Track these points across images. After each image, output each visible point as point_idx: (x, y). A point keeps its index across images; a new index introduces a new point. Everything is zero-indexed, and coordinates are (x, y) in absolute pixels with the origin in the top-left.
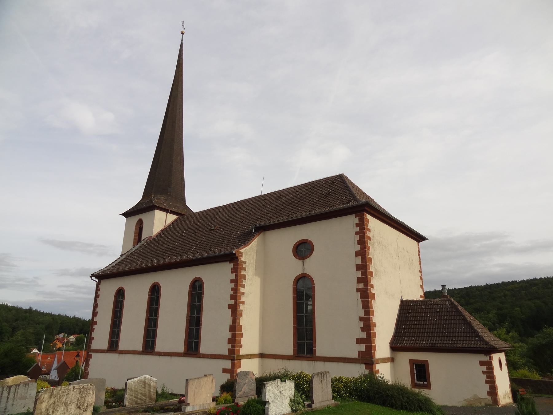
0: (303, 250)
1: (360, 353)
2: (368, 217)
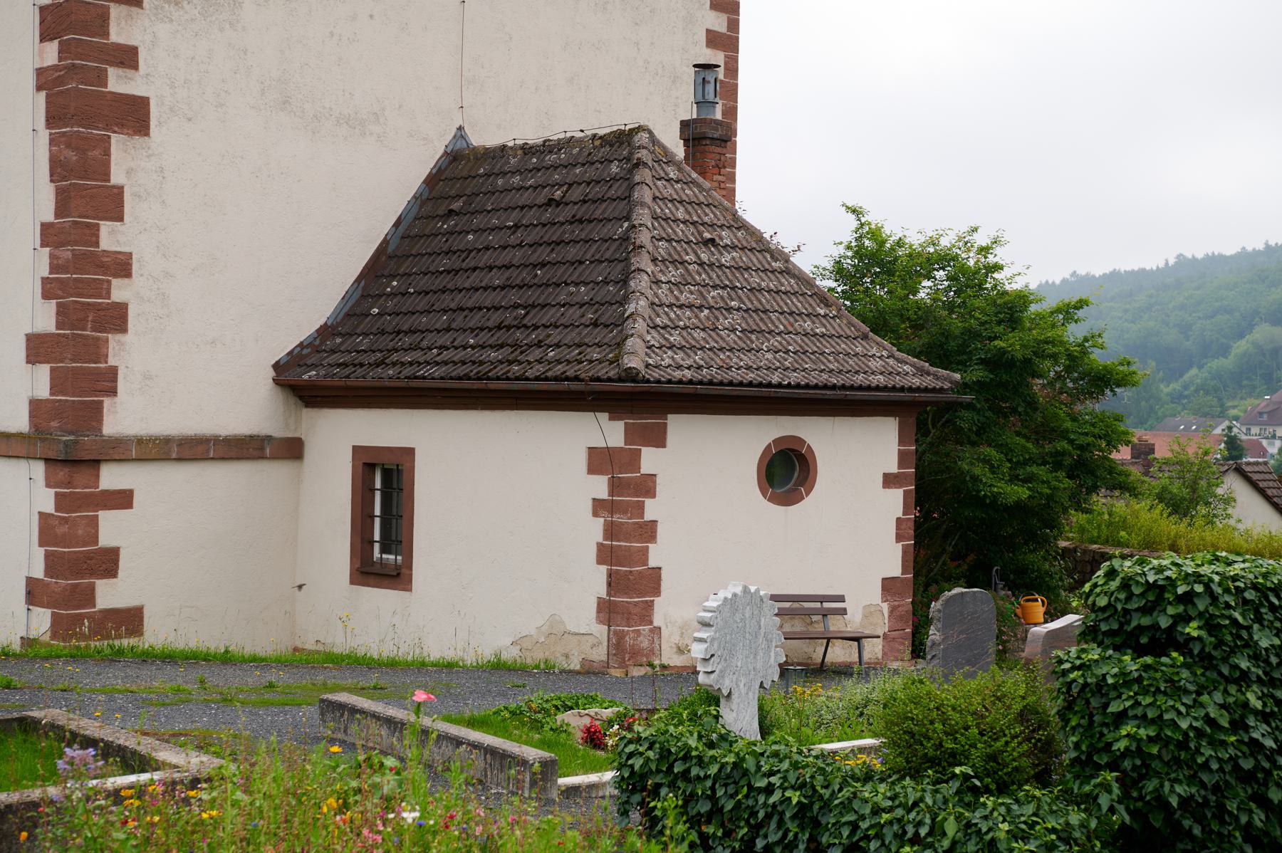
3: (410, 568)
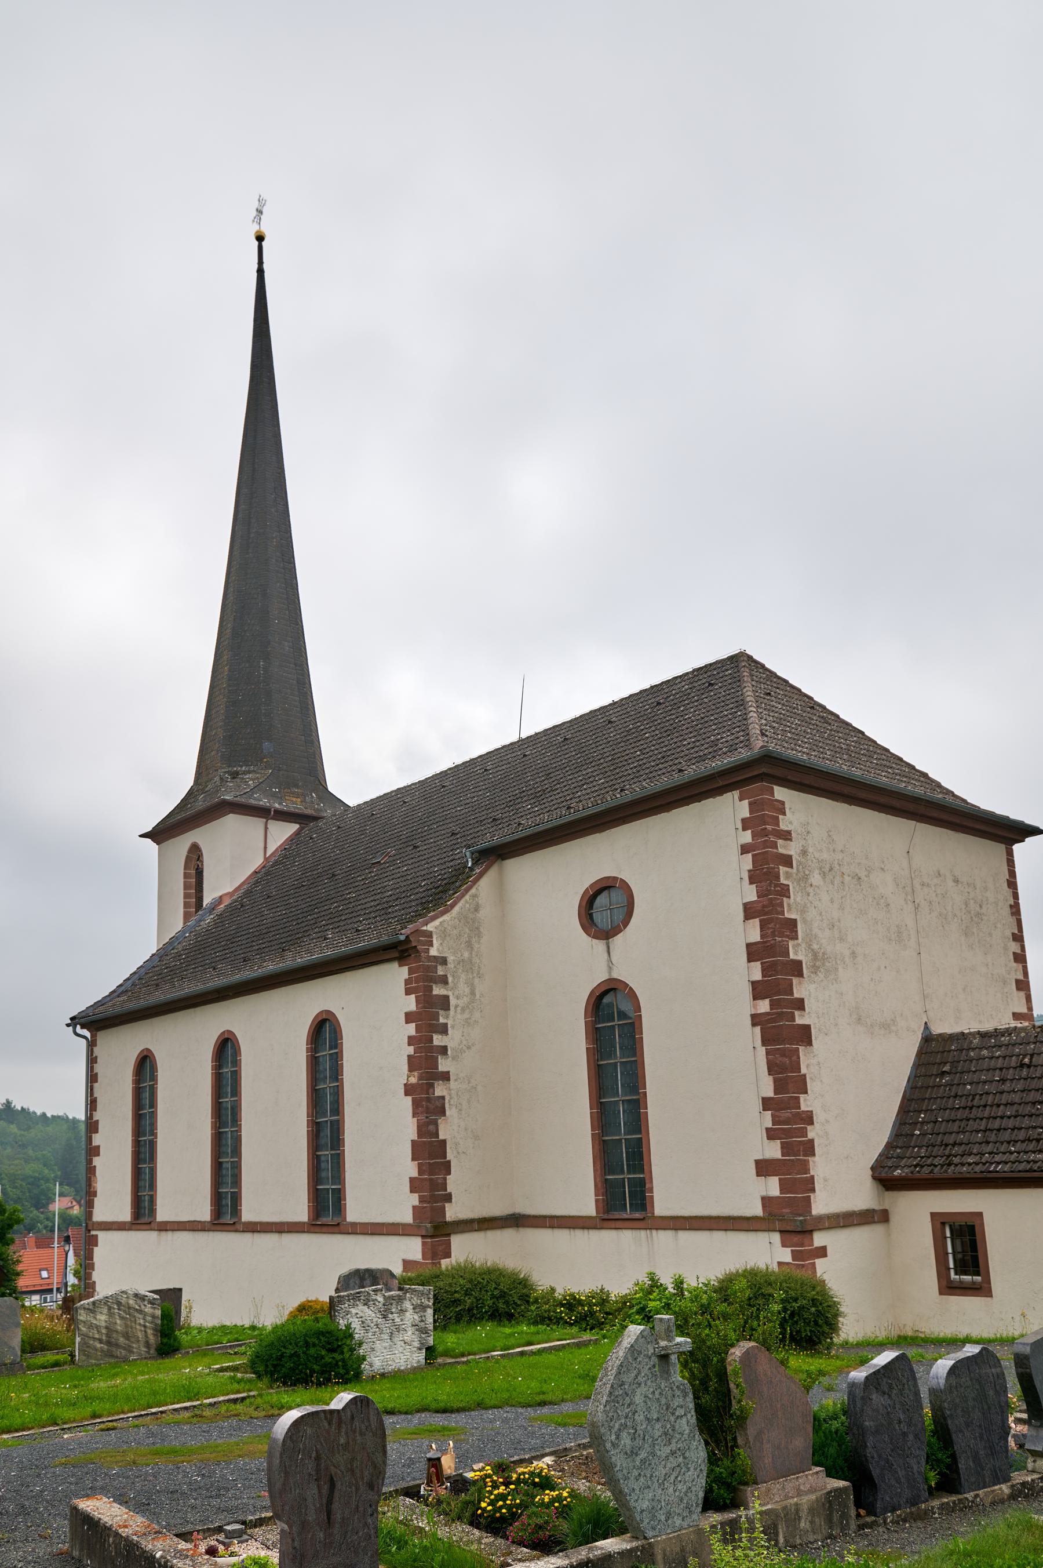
0: (605, 909)
1: (766, 1201)
2: (780, 793)
3: (989, 1283)
